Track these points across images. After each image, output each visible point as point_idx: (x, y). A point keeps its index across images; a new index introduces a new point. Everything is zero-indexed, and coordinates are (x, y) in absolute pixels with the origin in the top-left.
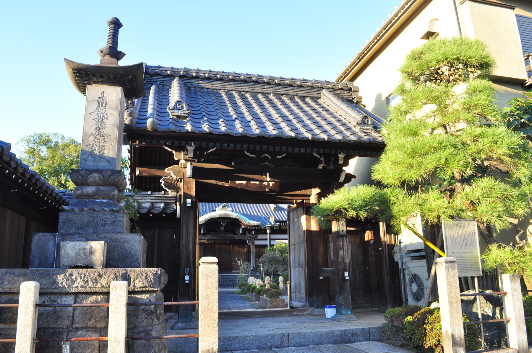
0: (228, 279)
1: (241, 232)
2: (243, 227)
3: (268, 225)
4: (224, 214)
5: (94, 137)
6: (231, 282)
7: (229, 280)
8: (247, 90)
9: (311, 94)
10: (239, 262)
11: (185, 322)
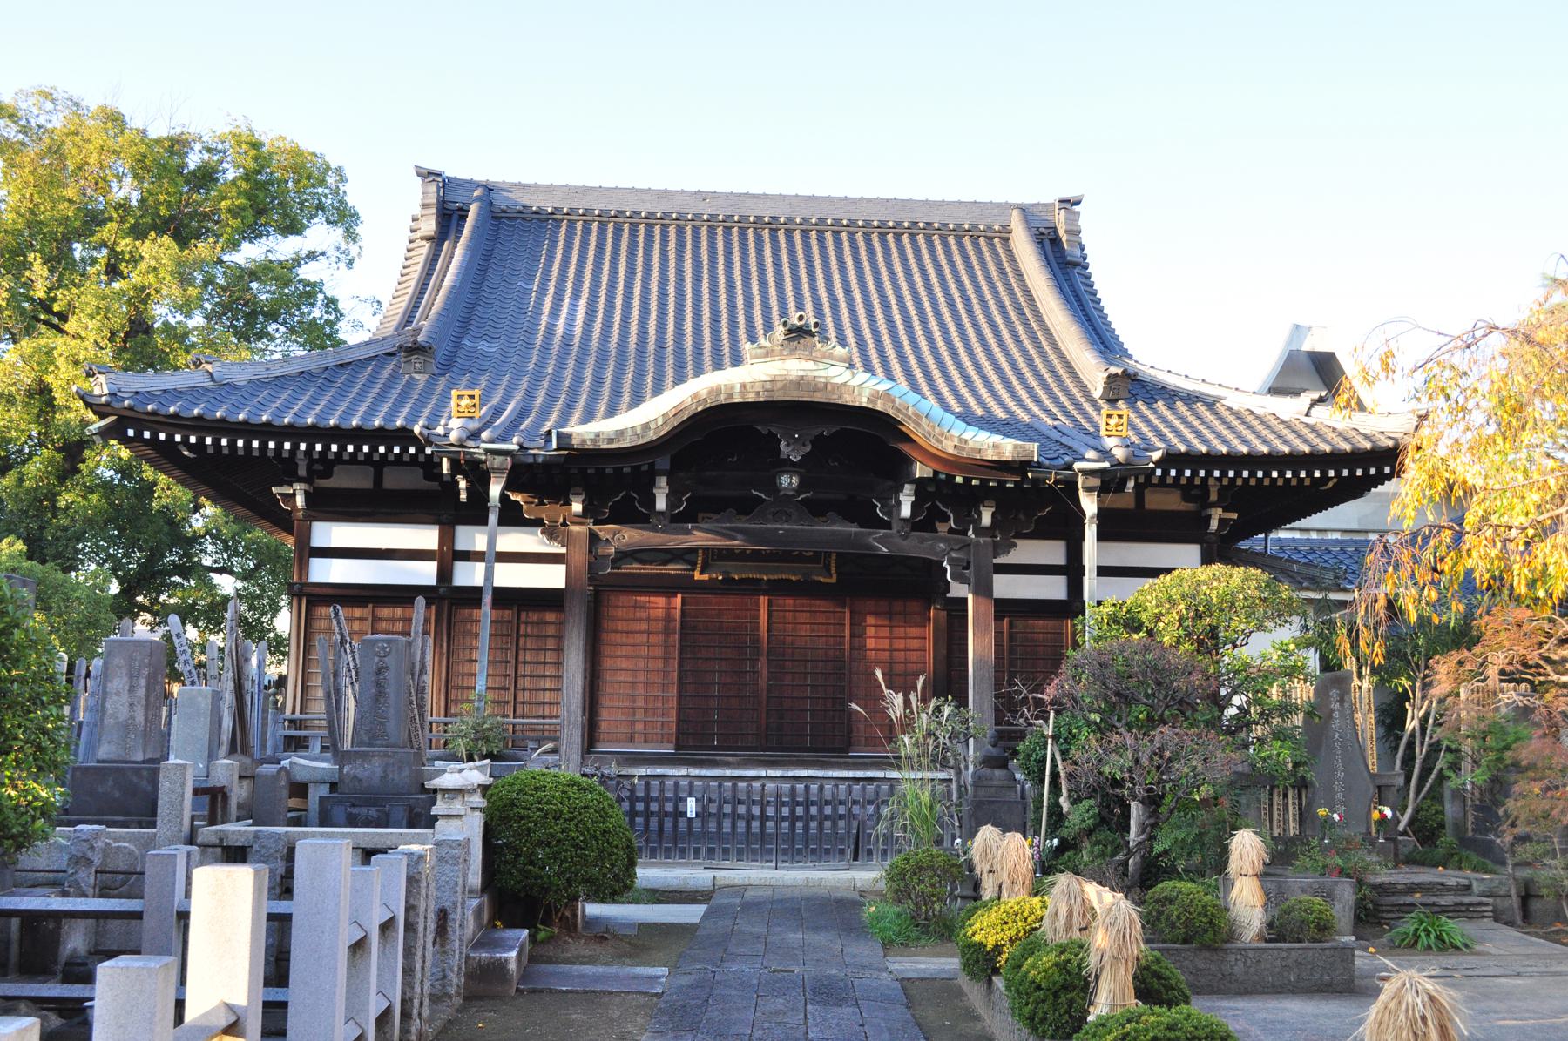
0: (835, 802)
1: (906, 511)
2: (921, 471)
3: (1090, 461)
4: (799, 383)
6: (841, 823)
7: (828, 810)
10: (898, 699)
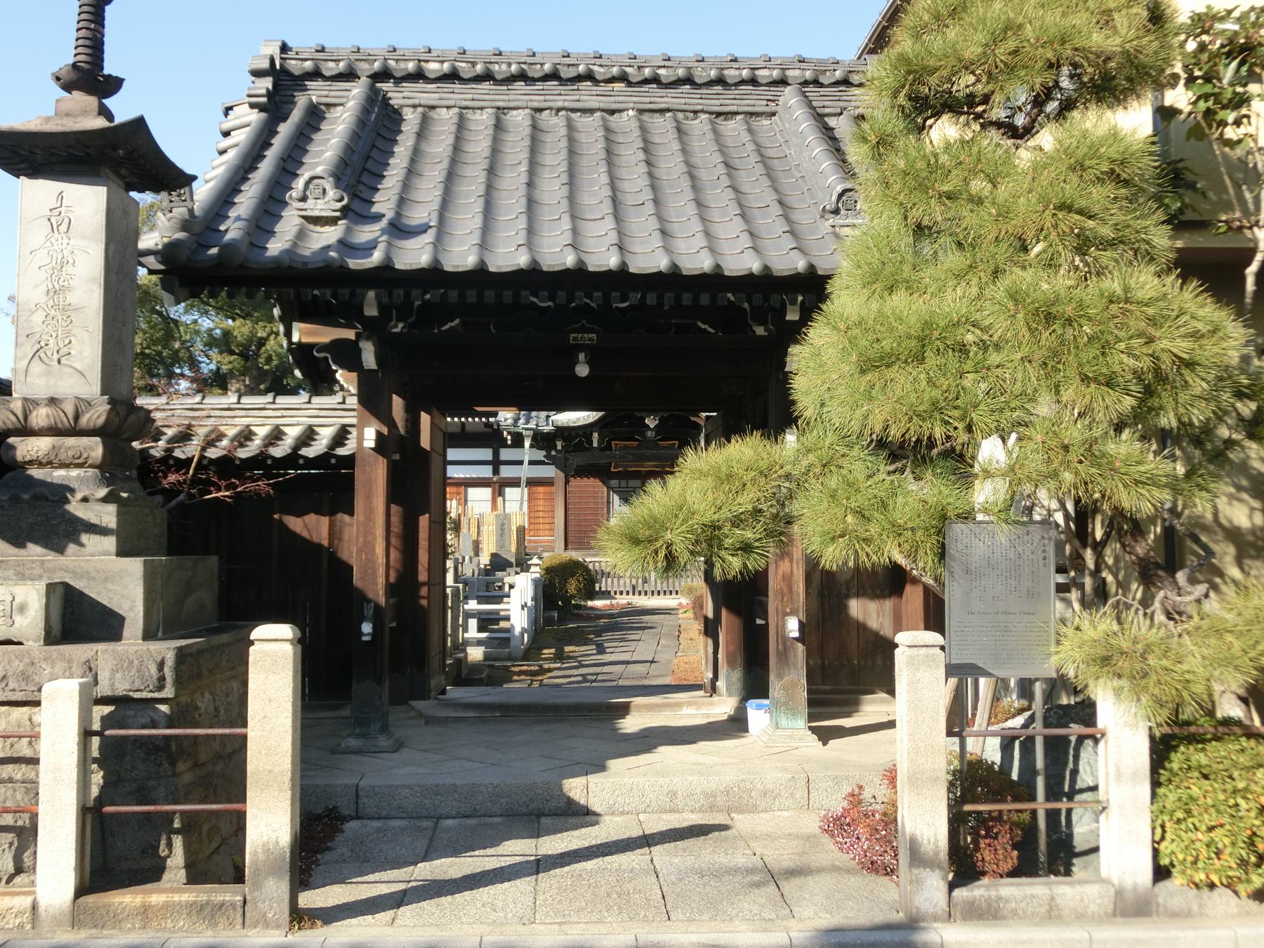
5: (44, 314)
8: (560, 104)
9: (749, 105)
11: (363, 736)
